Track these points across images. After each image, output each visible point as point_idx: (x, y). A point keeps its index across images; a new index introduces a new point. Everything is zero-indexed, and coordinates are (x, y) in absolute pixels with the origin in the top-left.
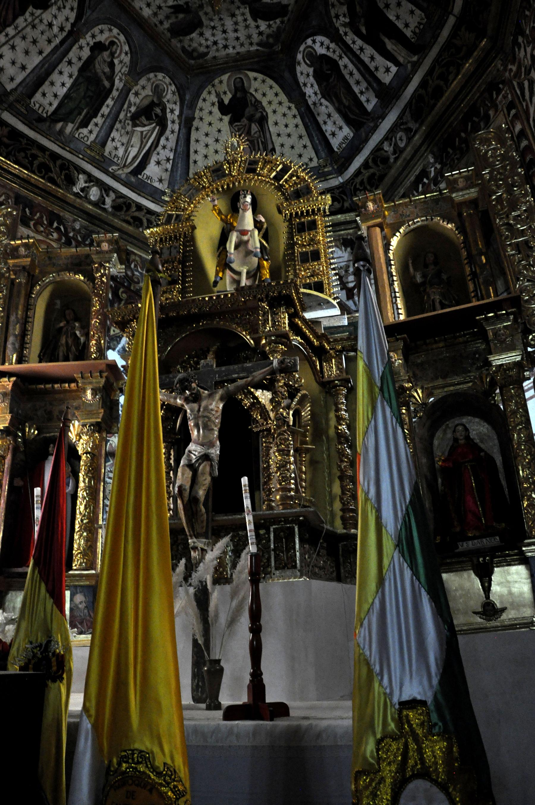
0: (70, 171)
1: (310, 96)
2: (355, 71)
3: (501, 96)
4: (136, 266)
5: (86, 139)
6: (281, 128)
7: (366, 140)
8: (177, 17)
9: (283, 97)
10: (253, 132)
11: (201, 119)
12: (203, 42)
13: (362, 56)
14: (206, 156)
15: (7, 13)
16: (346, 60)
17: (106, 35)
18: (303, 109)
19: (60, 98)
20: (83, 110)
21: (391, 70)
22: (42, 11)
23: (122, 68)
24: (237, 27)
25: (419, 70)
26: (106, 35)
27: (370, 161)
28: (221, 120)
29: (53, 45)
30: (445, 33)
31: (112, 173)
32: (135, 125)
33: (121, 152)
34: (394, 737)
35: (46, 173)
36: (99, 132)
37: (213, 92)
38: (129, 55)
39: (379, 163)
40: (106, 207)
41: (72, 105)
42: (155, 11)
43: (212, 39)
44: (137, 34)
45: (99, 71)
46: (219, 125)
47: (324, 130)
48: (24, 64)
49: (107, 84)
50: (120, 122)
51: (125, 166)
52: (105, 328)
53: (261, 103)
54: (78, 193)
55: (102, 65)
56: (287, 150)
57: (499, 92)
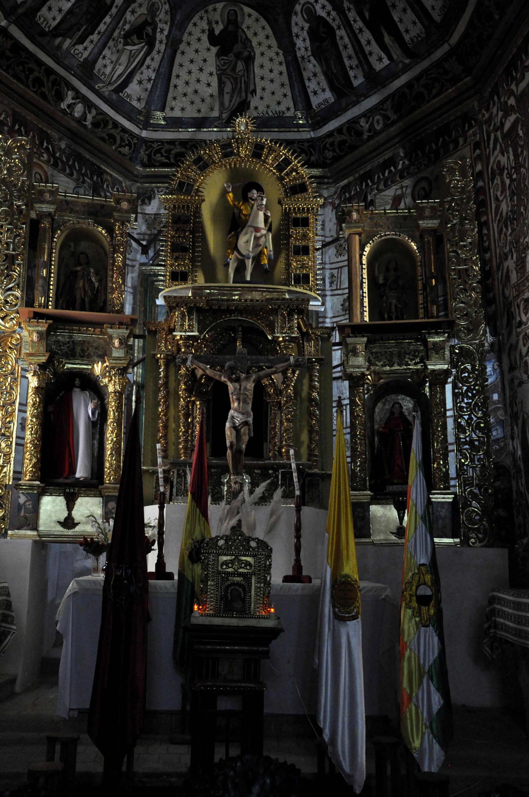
0: (60, 87)
1: (299, 49)
2: (350, 46)
3: (471, 132)
4: (107, 186)
5: (80, 55)
7: (346, 110)
9: (273, 41)
10: (238, 69)
11: (189, 44)
13: (359, 36)
14: (187, 83)
18: (290, 58)
19: (64, 13)
20: (83, 26)
21: (384, 60)
25: (409, 72)
27: (345, 128)
28: (209, 49)
30: (438, 54)
31: (97, 90)
32: (126, 44)
33: (108, 70)
34: (417, 574)
35: (39, 88)
36: (93, 49)
37: (205, 18)
40: (87, 123)
50: (114, 39)
51: (110, 83)
53: (251, 42)
54: (65, 109)
56: (267, 94)
57: (471, 127)
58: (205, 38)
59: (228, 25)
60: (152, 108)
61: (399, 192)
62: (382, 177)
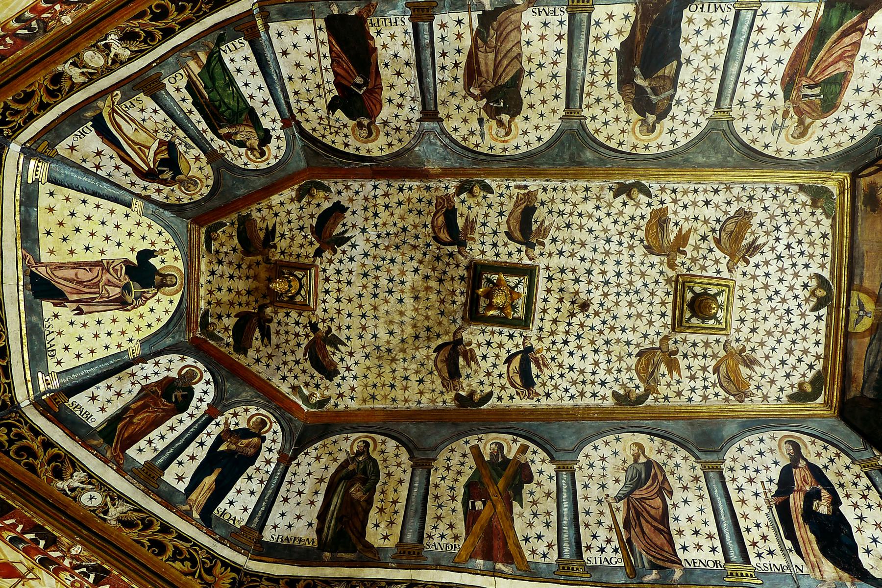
2: (176, 434)
5: (173, 80)
6: (107, 326)
12: (225, 249)
13: (194, 444)
15: (344, 69)
16: (188, 422)
17: (274, 152)
19: (234, 74)
26: (274, 152)
27: (56, 451)
30: (225, 552)
33: (135, 113)
35: (152, 12)
37: (167, 247)
38: (243, 166)
39: (54, 464)
41: (220, 83)
43: (226, 260)
44: (260, 182)
45: (242, 128)
46: (126, 247)
47: (99, 385)
49: (224, 131)
51: (114, 110)
54: (106, 39)
56: (78, 330)
58: (145, 245)
59: (161, 275)
60: (53, 165)
61: (23, 569)
62: (19, 529)
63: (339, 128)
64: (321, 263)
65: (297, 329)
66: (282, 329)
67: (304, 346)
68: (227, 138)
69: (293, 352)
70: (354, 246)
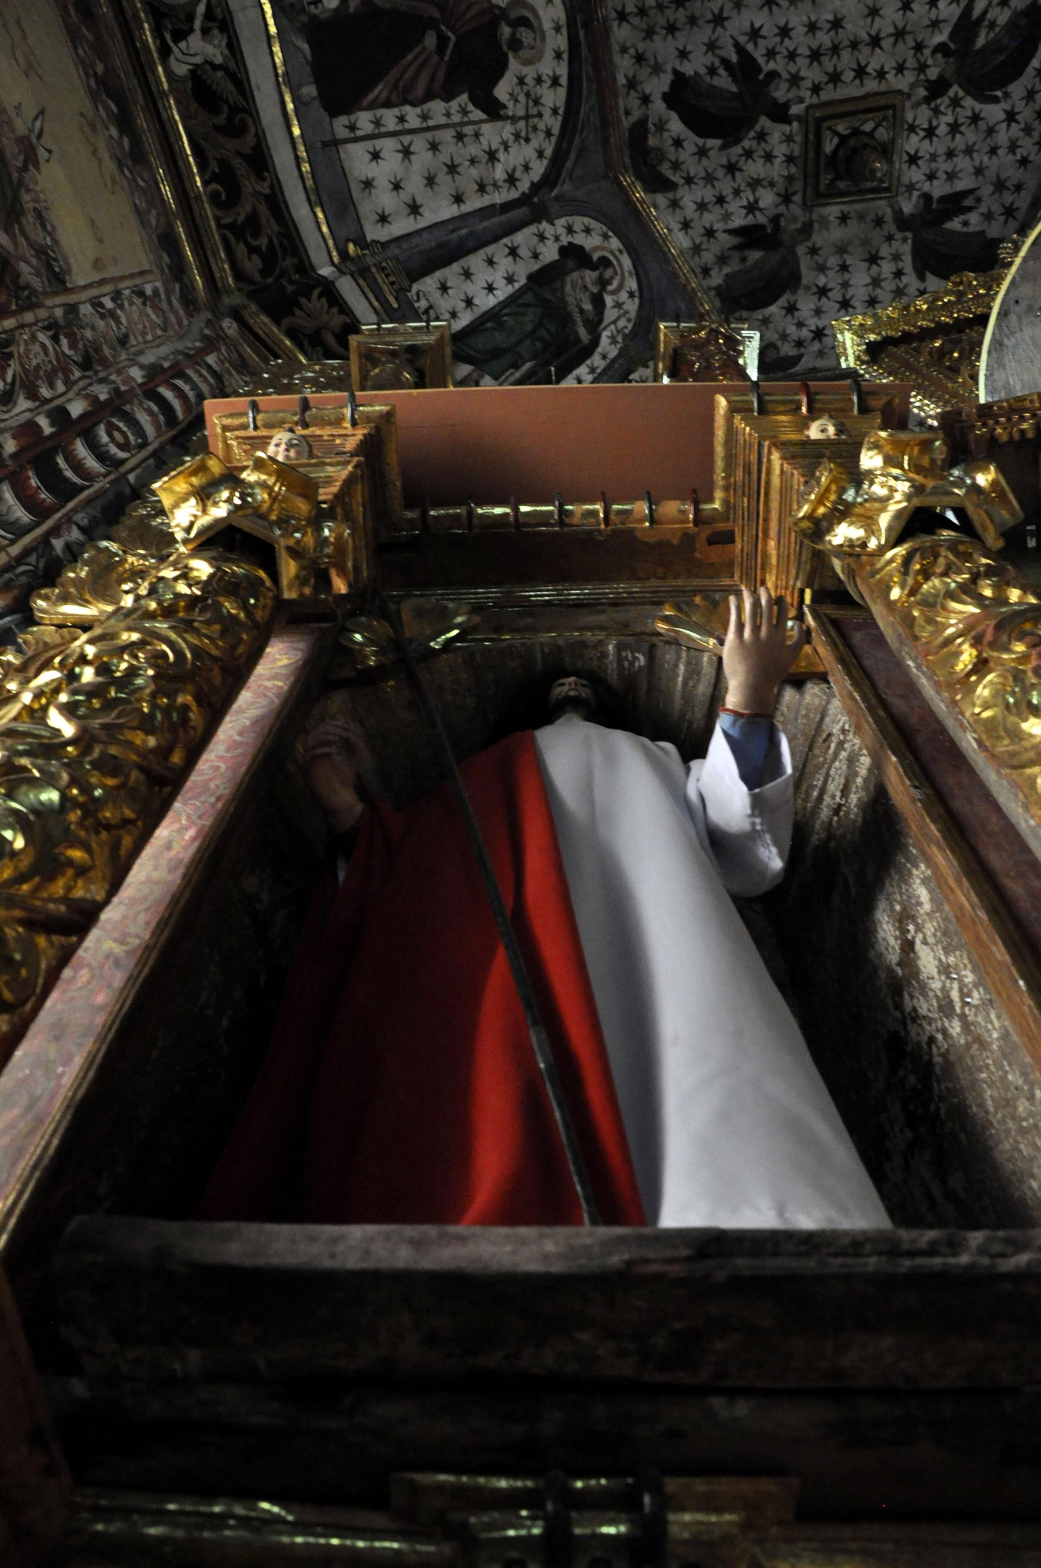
8: (743, 260)
12: (792, 329)
22: (484, 116)
23: (618, 318)
24: (878, 291)
29: (485, 201)
41: (500, 339)
42: (698, 241)
43: (813, 323)
48: (419, 201)
52: (798, 502)
55: (578, 290)
63: (528, 95)
64: (801, 100)
65: (942, 130)
66: (943, 166)
67: (978, 106)
68: (594, 325)
69: (991, 131)
70: (755, 34)
